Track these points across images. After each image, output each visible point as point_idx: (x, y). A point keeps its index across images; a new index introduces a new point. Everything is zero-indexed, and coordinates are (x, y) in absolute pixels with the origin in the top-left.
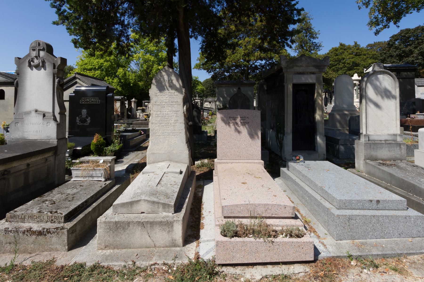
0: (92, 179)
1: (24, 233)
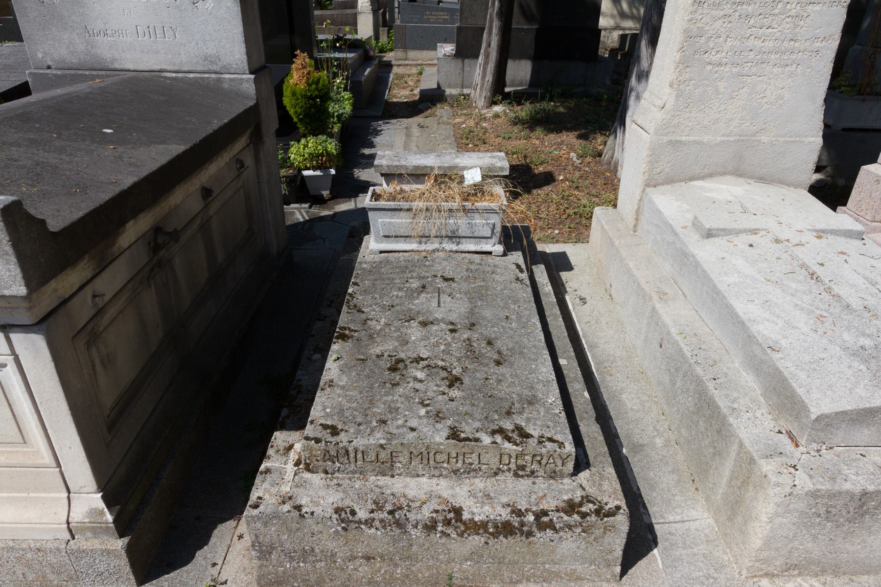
0: (454, 247)
1: (430, 527)
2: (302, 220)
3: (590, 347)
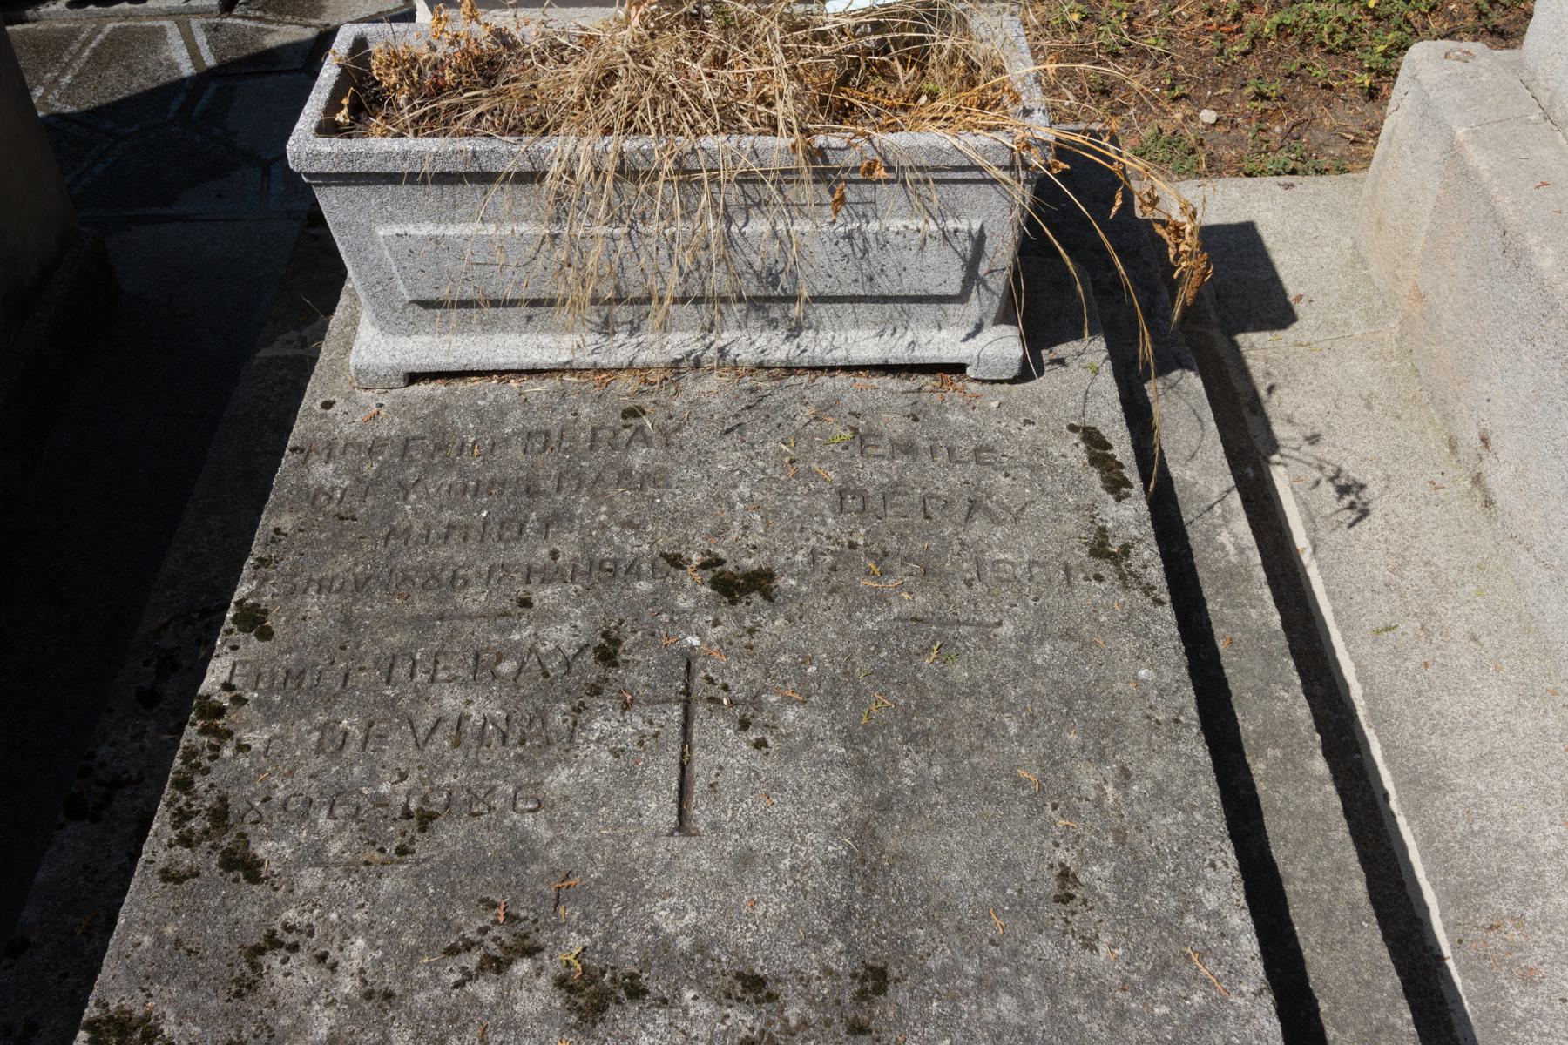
0: (779, 349)
2: (187, 70)
3: (1410, 781)
